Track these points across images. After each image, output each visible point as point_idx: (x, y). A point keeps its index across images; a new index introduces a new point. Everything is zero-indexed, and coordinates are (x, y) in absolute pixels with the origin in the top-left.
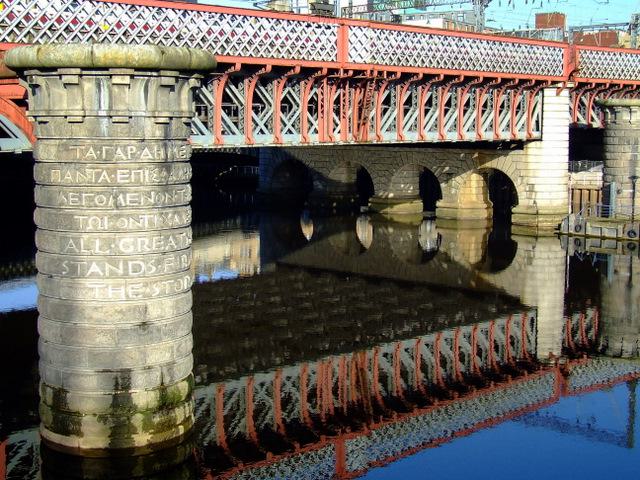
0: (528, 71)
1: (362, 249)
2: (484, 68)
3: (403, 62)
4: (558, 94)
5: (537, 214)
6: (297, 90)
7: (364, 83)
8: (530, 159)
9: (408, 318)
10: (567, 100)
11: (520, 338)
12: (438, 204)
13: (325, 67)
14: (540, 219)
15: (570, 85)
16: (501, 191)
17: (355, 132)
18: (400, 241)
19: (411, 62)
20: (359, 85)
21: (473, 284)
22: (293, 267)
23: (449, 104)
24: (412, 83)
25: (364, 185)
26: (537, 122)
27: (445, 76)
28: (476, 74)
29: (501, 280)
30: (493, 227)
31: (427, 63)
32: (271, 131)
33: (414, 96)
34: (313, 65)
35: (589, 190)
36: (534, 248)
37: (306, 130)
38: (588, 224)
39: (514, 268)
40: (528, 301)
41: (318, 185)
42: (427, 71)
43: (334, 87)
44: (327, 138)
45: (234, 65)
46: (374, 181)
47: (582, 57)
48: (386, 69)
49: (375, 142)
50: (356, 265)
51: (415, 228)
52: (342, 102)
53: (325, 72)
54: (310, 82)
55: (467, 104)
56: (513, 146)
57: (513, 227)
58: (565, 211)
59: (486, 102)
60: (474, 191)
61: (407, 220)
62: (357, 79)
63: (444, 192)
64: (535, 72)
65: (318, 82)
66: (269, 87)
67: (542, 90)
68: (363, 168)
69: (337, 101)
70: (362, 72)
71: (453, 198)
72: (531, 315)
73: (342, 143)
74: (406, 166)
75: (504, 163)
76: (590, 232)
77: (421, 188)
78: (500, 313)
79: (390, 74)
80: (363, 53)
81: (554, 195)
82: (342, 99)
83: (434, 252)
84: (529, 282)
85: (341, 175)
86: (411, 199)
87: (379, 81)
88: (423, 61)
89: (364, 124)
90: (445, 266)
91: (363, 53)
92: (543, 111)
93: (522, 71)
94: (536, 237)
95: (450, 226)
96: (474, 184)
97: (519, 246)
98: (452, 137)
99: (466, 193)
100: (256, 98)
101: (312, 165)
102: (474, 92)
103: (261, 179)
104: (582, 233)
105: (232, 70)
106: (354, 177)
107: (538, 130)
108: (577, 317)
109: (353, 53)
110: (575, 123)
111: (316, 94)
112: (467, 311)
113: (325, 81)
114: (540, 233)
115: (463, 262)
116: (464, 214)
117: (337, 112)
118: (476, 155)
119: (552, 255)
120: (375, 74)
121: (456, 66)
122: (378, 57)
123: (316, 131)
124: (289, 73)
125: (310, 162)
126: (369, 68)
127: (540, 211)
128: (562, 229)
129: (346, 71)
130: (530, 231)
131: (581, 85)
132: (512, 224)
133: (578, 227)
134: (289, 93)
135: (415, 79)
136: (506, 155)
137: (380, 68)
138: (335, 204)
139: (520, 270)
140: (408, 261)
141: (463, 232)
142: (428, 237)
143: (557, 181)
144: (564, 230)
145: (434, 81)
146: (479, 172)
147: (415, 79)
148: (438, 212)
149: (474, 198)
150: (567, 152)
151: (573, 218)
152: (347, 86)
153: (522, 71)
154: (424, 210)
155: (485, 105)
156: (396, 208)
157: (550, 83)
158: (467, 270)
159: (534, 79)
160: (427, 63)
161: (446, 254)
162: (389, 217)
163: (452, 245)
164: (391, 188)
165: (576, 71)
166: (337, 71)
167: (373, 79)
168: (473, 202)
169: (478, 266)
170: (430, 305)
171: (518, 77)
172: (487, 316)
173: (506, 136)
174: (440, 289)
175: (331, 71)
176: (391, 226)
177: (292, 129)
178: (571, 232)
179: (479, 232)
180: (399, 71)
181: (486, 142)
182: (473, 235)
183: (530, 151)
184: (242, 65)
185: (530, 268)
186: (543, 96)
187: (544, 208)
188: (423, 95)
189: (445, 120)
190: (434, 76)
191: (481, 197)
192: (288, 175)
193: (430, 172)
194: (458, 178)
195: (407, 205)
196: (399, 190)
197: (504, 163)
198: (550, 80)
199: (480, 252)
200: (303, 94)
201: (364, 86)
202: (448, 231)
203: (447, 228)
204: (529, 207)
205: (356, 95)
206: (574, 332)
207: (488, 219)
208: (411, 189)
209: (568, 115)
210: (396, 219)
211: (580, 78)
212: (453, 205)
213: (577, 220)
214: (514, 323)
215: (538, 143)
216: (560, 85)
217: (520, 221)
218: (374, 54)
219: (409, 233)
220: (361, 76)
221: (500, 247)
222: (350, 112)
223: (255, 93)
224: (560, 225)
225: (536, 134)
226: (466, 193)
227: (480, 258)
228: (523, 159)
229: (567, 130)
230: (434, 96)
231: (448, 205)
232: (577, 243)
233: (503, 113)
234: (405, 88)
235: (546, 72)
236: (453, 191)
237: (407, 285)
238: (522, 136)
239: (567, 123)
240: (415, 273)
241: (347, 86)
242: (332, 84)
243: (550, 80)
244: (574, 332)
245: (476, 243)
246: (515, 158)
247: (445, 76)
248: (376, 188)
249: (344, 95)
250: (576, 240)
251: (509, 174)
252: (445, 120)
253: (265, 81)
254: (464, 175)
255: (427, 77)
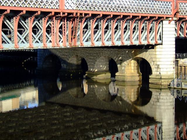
0: (154, 13)
1: (84, 94)
2: (133, 11)
3: (93, 9)
4: (169, 23)
5: (161, 78)
6: (41, 22)
7: (74, 19)
8: (157, 53)
9: (100, 128)
10: (174, 26)
11: (154, 136)
12: (117, 74)
13: (53, 11)
14: (162, 81)
15: (175, 19)
16: (145, 68)
17: (70, 42)
18: (100, 91)
19: (96, 9)
20: (71, 20)
21: (133, 111)
22: (53, 103)
23: (126, 28)
24: (108, 19)
25: (84, 66)
26: (160, 36)
27: (150, 17)
28: (72, 12)
29: (145, 109)
30: (142, 84)
31: (104, 9)
32: (42, 41)
33: (109, 25)
34: (182, 17)
35: (185, 67)
36: (160, 94)
37: (45, 40)
38: (183, 83)
39: (151, 103)
40: (158, 120)
41: (64, 66)
42: (104, 13)
43: (59, 21)
44: (56, 45)
45: (22, 11)
46: (88, 64)
47: (180, 6)
48: (84, 12)
49: (80, 46)
50: (81, 102)
51: (107, 85)
52: (63, 28)
53: (53, 14)
54: (47, 18)
55: (135, 28)
56: (150, 47)
57: (150, 85)
58: (172, 77)
59: (151, 27)
60: (132, 68)
61: (103, 82)
62: (69, 17)
63: (119, 69)
64: (157, 13)
65: (51, 18)
66: (26, 21)
67: (162, 21)
68: (84, 58)
69: (61, 27)
70: (72, 14)
71: (123, 72)
72: (159, 125)
73: (63, 47)
74: (102, 57)
75: (145, 55)
76: (183, 87)
77: (110, 67)
78: (146, 125)
79: (86, 14)
80: (72, 5)
81: (168, 70)
82: (63, 26)
83: (115, 96)
84: (158, 110)
85: (74, 61)
86: (105, 72)
87: (81, 18)
88: (164, 12)
89: (74, 38)
90: (120, 102)
91: (72, 5)
92: (162, 31)
93: (152, 12)
94: (161, 89)
95: (122, 84)
96: (132, 65)
97: (153, 93)
98: (119, 43)
99: (129, 69)
100: (20, 26)
101: (61, 56)
102: (129, 22)
103: (38, 63)
104: (180, 87)
105: (21, 13)
106: (80, 62)
107: (160, 40)
108: (181, 126)
109: (67, 5)
110: (178, 37)
111: (50, 24)
112: (130, 124)
113: (54, 18)
114: (163, 87)
115: (128, 101)
116: (128, 79)
117: (61, 32)
118: (133, 52)
119: (168, 98)
120: (79, 14)
121: (119, 10)
122: (80, 7)
123: (50, 41)
124: (35, 14)
125: (58, 54)
126: (75, 12)
127: (162, 77)
128: (171, 86)
129: (64, 13)
130: (157, 86)
131: (180, 19)
132: (149, 83)
133: (178, 85)
134: (37, 23)
135: (109, 17)
136: (146, 51)
137: (81, 12)
138: (71, 75)
139: (153, 105)
140: (104, 100)
141: (128, 87)
142: (113, 89)
143: (170, 63)
144: (172, 86)
145: (136, 19)
146: (135, 59)
147: (109, 17)
148: (116, 78)
149: (133, 71)
150: (174, 49)
151: (176, 80)
152: (66, 21)
153: (152, 12)
154: (111, 77)
155: (143, 29)
156: (98, 76)
157: (165, 18)
158: (130, 104)
159: (157, 16)
160: (104, 9)
161: (120, 97)
162: (94, 80)
163: (123, 93)
164: (95, 66)
165: (177, 12)
166: (59, 13)
167: (78, 17)
168: (132, 73)
169: (135, 103)
170: (113, 121)
171: (149, 15)
172: (139, 126)
173: (145, 43)
174: (118, 114)
175: (56, 13)
176: (97, 85)
177: (39, 41)
178: (175, 87)
179: (135, 87)
180: (90, 13)
181: (135, 45)
182: (132, 88)
183: (157, 50)
184: (26, 11)
185: (158, 104)
186: (163, 24)
187: (164, 76)
188: (113, 25)
189: (133, 36)
190: (118, 16)
191: (136, 71)
192: (51, 61)
193: (114, 57)
194: (125, 63)
195: (103, 75)
196: (99, 68)
197: (145, 55)
198: (165, 17)
199: (136, 96)
200: (43, 24)
201: (74, 20)
202: (121, 87)
203: (121, 85)
204: (157, 75)
205: (70, 25)
206: (180, 133)
207: (139, 81)
208: (105, 67)
209: (175, 33)
210: (98, 81)
211: (180, 15)
212: (123, 75)
213: (178, 81)
214: (151, 130)
215: (161, 46)
216: (170, 19)
217: (153, 82)
218: (78, 5)
219: (105, 87)
220: (71, 16)
221: (145, 94)
222: (68, 32)
223: (19, 23)
224: (170, 84)
225: (159, 42)
226: (129, 69)
227: (136, 99)
228: (154, 53)
229: (174, 40)
230: (119, 25)
231: (121, 75)
232: (178, 92)
233: (135, 33)
234: (105, 21)
235: (163, 13)
236: (123, 68)
237: (103, 112)
238: (153, 42)
239: (175, 37)
240: (107, 106)
241: (66, 21)
242: (58, 20)
243: (165, 17)
244: (180, 133)
245: (134, 92)
246: (151, 53)
247: (150, 17)
248: (89, 67)
249: (64, 24)
250: (177, 91)
251: (148, 60)
252: (133, 36)
253: (24, 18)
254: (128, 61)
255: (115, 17)
